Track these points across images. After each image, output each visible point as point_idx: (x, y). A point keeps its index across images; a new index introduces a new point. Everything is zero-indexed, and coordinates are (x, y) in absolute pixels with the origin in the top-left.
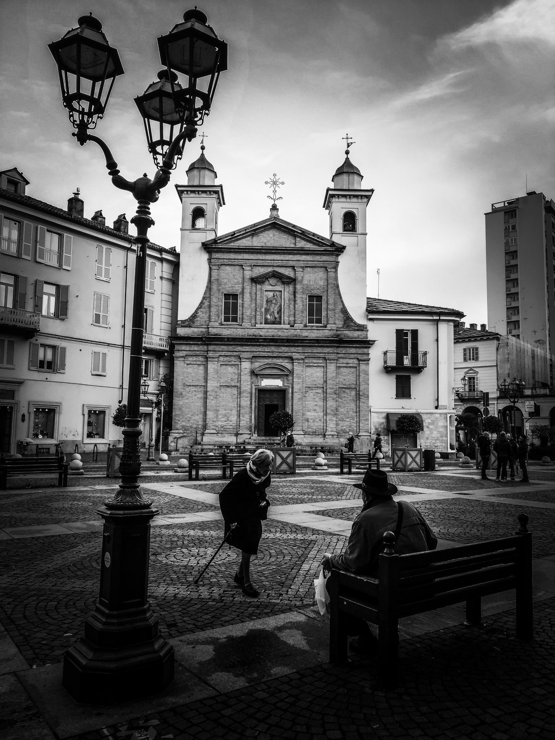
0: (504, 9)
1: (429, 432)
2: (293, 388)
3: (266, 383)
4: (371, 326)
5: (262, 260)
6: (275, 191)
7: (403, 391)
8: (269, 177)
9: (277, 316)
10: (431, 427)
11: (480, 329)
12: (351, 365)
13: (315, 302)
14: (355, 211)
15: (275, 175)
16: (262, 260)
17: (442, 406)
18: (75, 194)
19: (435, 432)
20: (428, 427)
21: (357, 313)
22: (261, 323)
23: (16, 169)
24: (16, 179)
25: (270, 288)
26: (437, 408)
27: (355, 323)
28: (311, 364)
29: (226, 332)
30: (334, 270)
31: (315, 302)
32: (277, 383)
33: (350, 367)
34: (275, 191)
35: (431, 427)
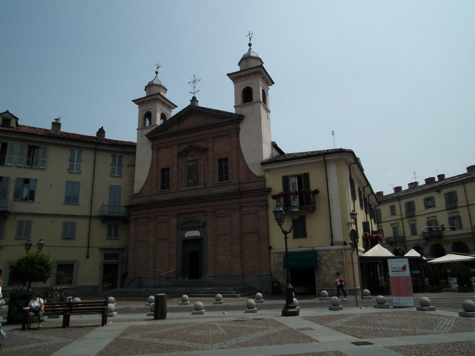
0: (172, 299)
1: (326, 269)
2: (207, 237)
3: (189, 234)
4: (268, 177)
5: (176, 140)
6: (194, 87)
7: (300, 231)
8: (190, 79)
9: (195, 179)
10: (328, 263)
11: (438, 180)
12: (252, 212)
13: (223, 163)
14: (250, 86)
15: (194, 76)
16: (176, 140)
17: (337, 242)
18: (56, 119)
19: (332, 269)
20: (325, 264)
21: (257, 171)
22: (185, 187)
23: (8, 111)
24: (8, 118)
25: (191, 159)
26: (332, 244)
27: (254, 175)
28: (221, 215)
29: (161, 198)
30: (236, 135)
31: (223, 163)
32: (196, 233)
33: (252, 214)
34: (194, 87)
35: (328, 263)
